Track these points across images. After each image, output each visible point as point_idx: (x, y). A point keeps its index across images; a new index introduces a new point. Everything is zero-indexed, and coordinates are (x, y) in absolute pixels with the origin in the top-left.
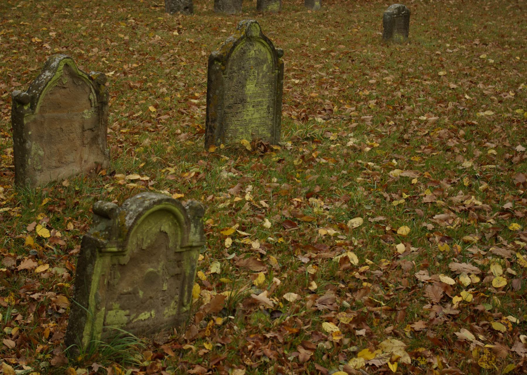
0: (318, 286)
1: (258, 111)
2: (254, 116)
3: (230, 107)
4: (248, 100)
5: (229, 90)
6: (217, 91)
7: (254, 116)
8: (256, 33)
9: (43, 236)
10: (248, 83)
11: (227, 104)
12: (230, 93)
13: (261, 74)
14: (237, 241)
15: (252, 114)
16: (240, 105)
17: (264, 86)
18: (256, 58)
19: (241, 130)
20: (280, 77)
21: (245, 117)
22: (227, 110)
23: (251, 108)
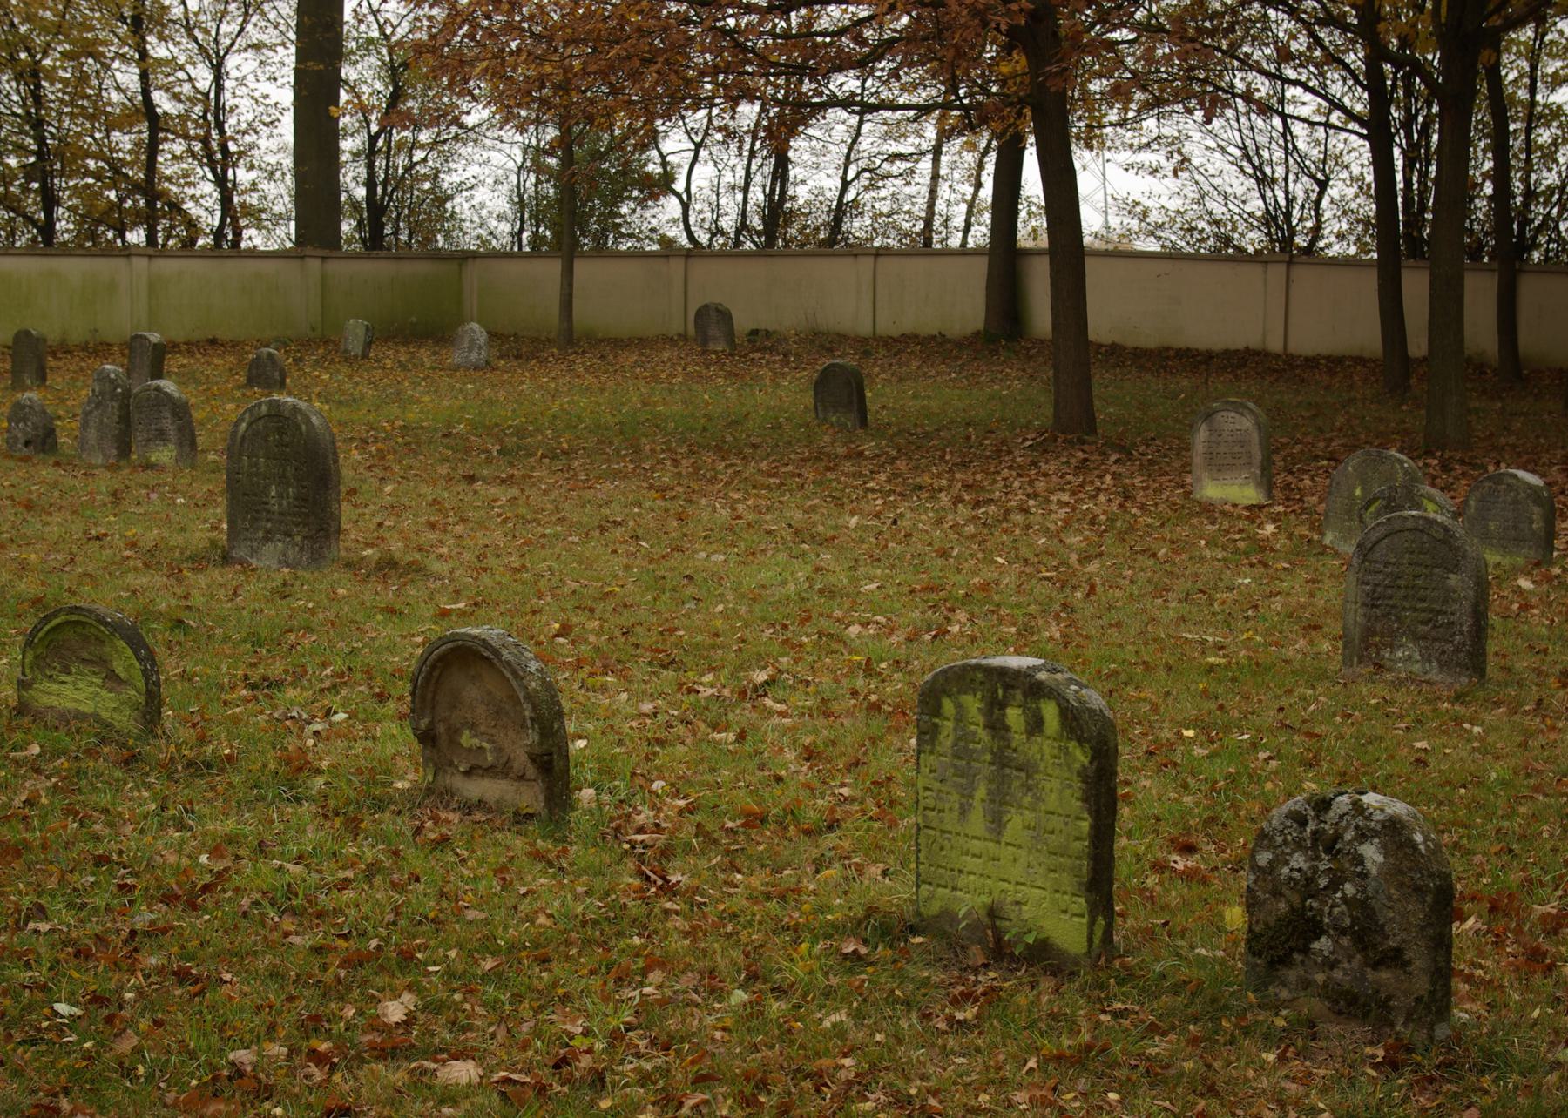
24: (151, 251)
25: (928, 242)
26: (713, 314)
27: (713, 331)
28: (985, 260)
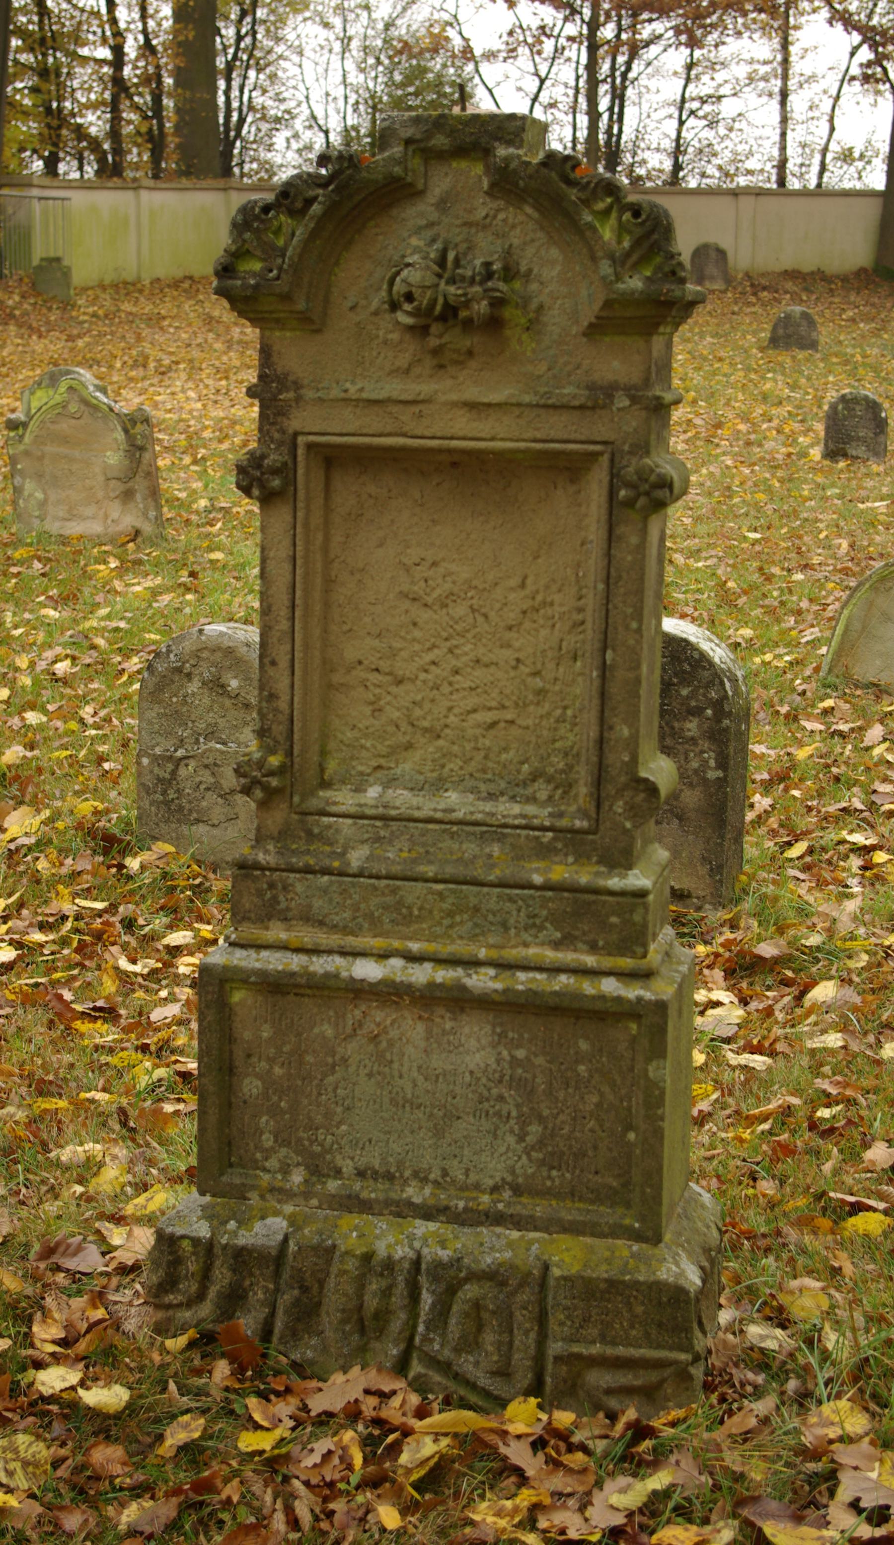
24: (782, 190)
25: (781, 182)
26: (713, 254)
27: (711, 269)
28: (879, 201)
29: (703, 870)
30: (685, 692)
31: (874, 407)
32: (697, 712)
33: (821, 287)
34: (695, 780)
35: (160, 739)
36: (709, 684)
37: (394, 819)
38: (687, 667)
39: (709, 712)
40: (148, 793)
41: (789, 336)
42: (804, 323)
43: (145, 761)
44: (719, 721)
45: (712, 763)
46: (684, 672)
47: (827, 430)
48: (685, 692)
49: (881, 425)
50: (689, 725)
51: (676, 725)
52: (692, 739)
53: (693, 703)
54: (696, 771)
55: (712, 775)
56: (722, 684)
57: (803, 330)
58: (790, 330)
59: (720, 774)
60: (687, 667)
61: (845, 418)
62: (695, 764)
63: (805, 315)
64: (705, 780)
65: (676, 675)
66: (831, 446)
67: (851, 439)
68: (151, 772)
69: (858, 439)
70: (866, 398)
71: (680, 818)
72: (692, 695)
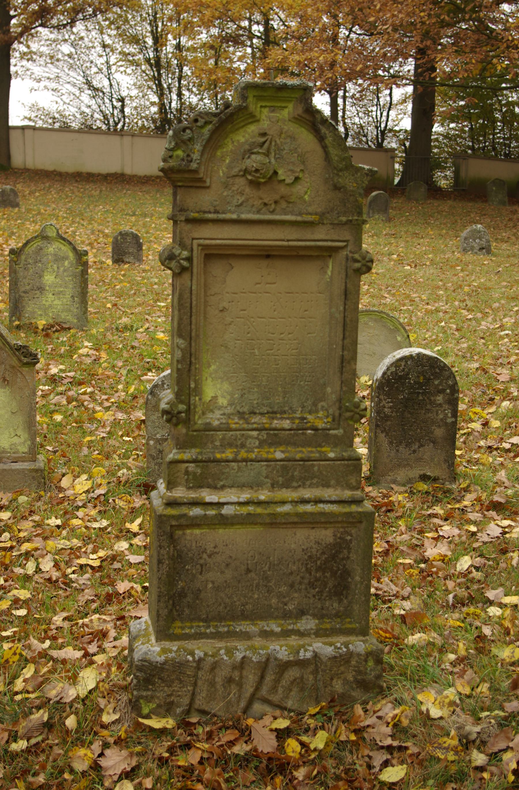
0: (324, 748)
1: (59, 299)
2: (55, 303)
3: (25, 292)
4: (47, 288)
5: (25, 278)
6: (75, 356)
7: (55, 303)
8: (52, 233)
9: (450, 248)
10: (46, 274)
11: (23, 289)
12: (26, 281)
13: (62, 269)
14: (77, 93)
15: (52, 301)
16: (38, 292)
17: (67, 279)
18: (55, 255)
19: (39, 313)
20: (84, 273)
21: (44, 302)
22: (22, 294)
23: (51, 295)
29: (445, 466)
30: (436, 382)
31: (136, 238)
32: (443, 391)
33: (57, 178)
34: (441, 424)
35: (159, 430)
36: (449, 378)
37: (252, 460)
38: (437, 370)
39: (448, 391)
40: (153, 459)
41: (5, 201)
42: (12, 194)
43: (152, 442)
44: (453, 395)
45: (450, 415)
46: (436, 373)
47: (113, 249)
48: (436, 382)
49: (140, 246)
50: (438, 398)
51: (432, 398)
52: (440, 404)
53: (441, 387)
54: (442, 420)
55: (449, 420)
56: (454, 377)
57: (12, 197)
58: (5, 198)
59: (453, 420)
60: (437, 370)
61: (122, 243)
62: (441, 416)
63: (12, 190)
64: (446, 423)
65: (432, 375)
66: (116, 257)
67: (125, 253)
68: (155, 448)
69: (129, 253)
70: (132, 233)
71: (434, 443)
72: (440, 384)
